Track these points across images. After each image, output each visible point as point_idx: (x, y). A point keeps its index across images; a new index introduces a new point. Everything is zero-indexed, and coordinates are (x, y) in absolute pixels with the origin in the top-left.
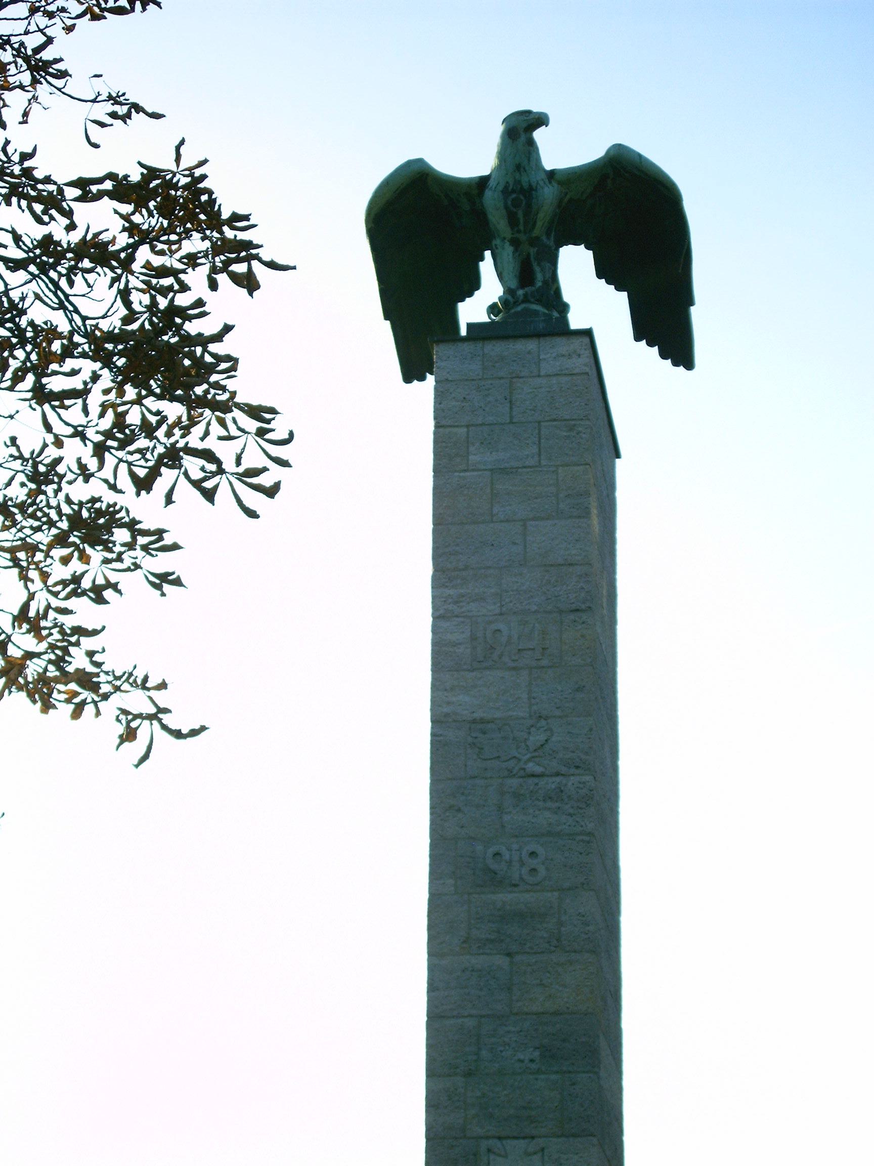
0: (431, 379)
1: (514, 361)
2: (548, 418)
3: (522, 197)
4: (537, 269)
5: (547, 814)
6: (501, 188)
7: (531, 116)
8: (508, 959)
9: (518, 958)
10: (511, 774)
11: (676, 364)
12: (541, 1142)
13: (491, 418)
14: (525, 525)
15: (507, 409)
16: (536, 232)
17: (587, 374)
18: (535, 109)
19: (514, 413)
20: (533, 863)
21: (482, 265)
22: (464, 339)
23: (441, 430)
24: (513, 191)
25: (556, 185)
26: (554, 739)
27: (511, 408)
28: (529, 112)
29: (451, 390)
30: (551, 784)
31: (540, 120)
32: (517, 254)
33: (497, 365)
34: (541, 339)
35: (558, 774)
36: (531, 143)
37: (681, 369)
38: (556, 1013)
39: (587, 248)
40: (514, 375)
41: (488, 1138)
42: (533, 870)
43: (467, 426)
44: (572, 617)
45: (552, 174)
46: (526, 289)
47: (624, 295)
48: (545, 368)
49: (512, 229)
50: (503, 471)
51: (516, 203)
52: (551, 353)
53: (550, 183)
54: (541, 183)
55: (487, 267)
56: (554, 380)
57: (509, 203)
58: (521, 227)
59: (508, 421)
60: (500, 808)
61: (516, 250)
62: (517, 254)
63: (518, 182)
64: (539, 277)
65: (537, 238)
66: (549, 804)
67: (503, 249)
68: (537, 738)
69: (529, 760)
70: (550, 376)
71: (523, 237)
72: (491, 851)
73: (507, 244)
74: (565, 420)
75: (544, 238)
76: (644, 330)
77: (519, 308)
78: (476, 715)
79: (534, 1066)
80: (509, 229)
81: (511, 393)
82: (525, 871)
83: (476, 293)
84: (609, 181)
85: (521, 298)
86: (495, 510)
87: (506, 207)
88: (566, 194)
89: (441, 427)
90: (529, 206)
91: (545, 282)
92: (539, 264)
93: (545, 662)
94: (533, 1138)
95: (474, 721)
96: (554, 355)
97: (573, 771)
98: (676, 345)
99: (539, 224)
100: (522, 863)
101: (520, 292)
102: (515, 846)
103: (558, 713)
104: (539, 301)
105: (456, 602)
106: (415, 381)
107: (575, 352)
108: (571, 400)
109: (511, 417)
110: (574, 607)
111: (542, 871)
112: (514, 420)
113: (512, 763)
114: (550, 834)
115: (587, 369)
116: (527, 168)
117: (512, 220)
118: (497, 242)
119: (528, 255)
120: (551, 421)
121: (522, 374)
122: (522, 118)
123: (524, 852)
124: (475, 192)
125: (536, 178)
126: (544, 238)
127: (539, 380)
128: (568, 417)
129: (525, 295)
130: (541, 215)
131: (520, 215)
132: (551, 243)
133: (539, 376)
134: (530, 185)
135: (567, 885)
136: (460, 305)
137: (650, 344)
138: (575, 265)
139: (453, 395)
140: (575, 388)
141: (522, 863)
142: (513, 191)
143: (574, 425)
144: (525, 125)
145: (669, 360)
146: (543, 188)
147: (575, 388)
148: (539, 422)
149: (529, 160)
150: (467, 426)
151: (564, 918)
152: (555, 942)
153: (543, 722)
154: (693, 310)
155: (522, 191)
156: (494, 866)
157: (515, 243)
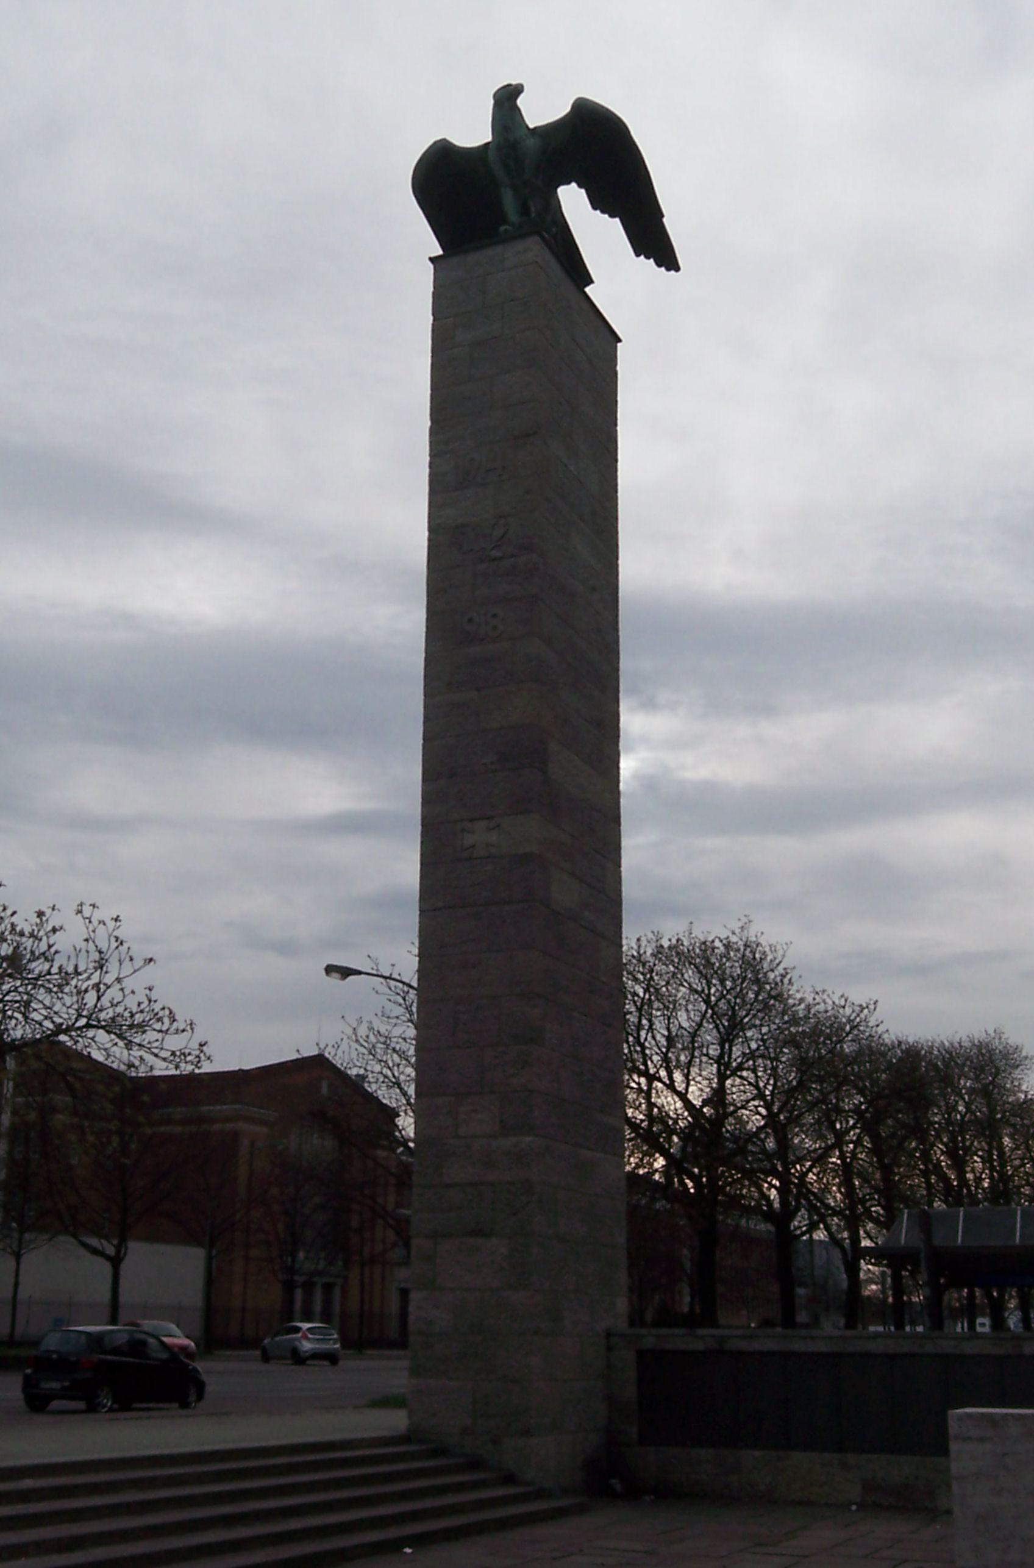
11: (668, 269)
18: (514, 83)
31: (518, 90)
35: (512, 556)
37: (673, 272)
42: (495, 628)
47: (617, 220)
137: (647, 257)
154: (664, 220)
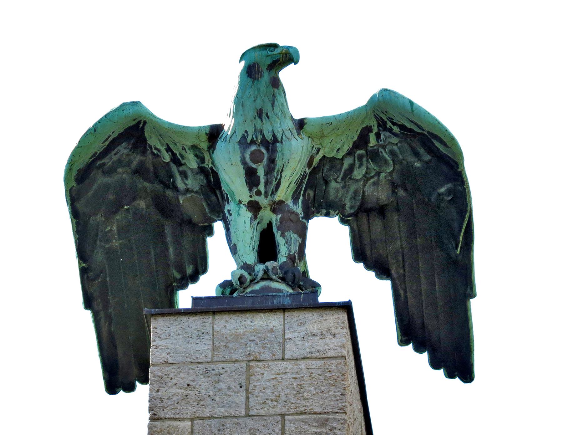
0: (142, 391)
1: (253, 341)
2: (294, 411)
3: (264, 150)
6: (238, 137)
7: (277, 51)
11: (450, 375)
13: (222, 410)
15: (244, 399)
16: (280, 195)
17: (344, 357)
18: (282, 43)
19: (251, 404)
21: (210, 241)
22: (186, 313)
23: (158, 423)
24: (253, 142)
25: (306, 138)
27: (247, 398)
28: (275, 46)
29: (171, 375)
31: (288, 57)
32: (256, 222)
33: (230, 345)
34: (287, 314)
36: (276, 83)
40: (252, 358)
43: (192, 420)
45: (301, 124)
46: (268, 264)
47: (387, 285)
48: (291, 350)
49: (250, 190)
52: (301, 331)
53: (299, 134)
54: (288, 134)
55: (216, 244)
56: (302, 364)
57: (247, 157)
58: (262, 188)
59: (243, 413)
62: (256, 222)
65: (281, 202)
67: (239, 214)
70: (297, 359)
71: (263, 201)
74: (315, 413)
75: (290, 202)
76: (411, 332)
77: (257, 287)
80: (246, 189)
81: (248, 379)
85: (261, 274)
87: (244, 162)
88: (318, 151)
89: (159, 419)
90: (272, 161)
91: (291, 258)
92: (283, 235)
96: (302, 334)
98: (450, 350)
99: (284, 185)
101: (260, 268)
104: (283, 279)
106: (122, 392)
107: (329, 330)
108: (323, 388)
109: (248, 409)
112: (251, 413)
115: (345, 352)
116: (270, 115)
117: (251, 178)
118: (230, 207)
119: (270, 224)
120: (297, 414)
121: (263, 357)
122: (264, 53)
125: (283, 127)
126: (290, 202)
127: (284, 364)
128: (319, 410)
129: (266, 272)
130: (287, 173)
131: (261, 172)
132: (299, 209)
133: (283, 359)
134: (274, 136)
137: (419, 349)
138: (328, 249)
139: (174, 381)
140: (328, 375)
142: (253, 142)
143: (327, 420)
144: (269, 61)
145: (442, 371)
146: (289, 140)
147: (328, 375)
148: (283, 416)
149: (273, 104)
150: (192, 420)
154: (473, 302)
155: (264, 143)
157: (254, 207)
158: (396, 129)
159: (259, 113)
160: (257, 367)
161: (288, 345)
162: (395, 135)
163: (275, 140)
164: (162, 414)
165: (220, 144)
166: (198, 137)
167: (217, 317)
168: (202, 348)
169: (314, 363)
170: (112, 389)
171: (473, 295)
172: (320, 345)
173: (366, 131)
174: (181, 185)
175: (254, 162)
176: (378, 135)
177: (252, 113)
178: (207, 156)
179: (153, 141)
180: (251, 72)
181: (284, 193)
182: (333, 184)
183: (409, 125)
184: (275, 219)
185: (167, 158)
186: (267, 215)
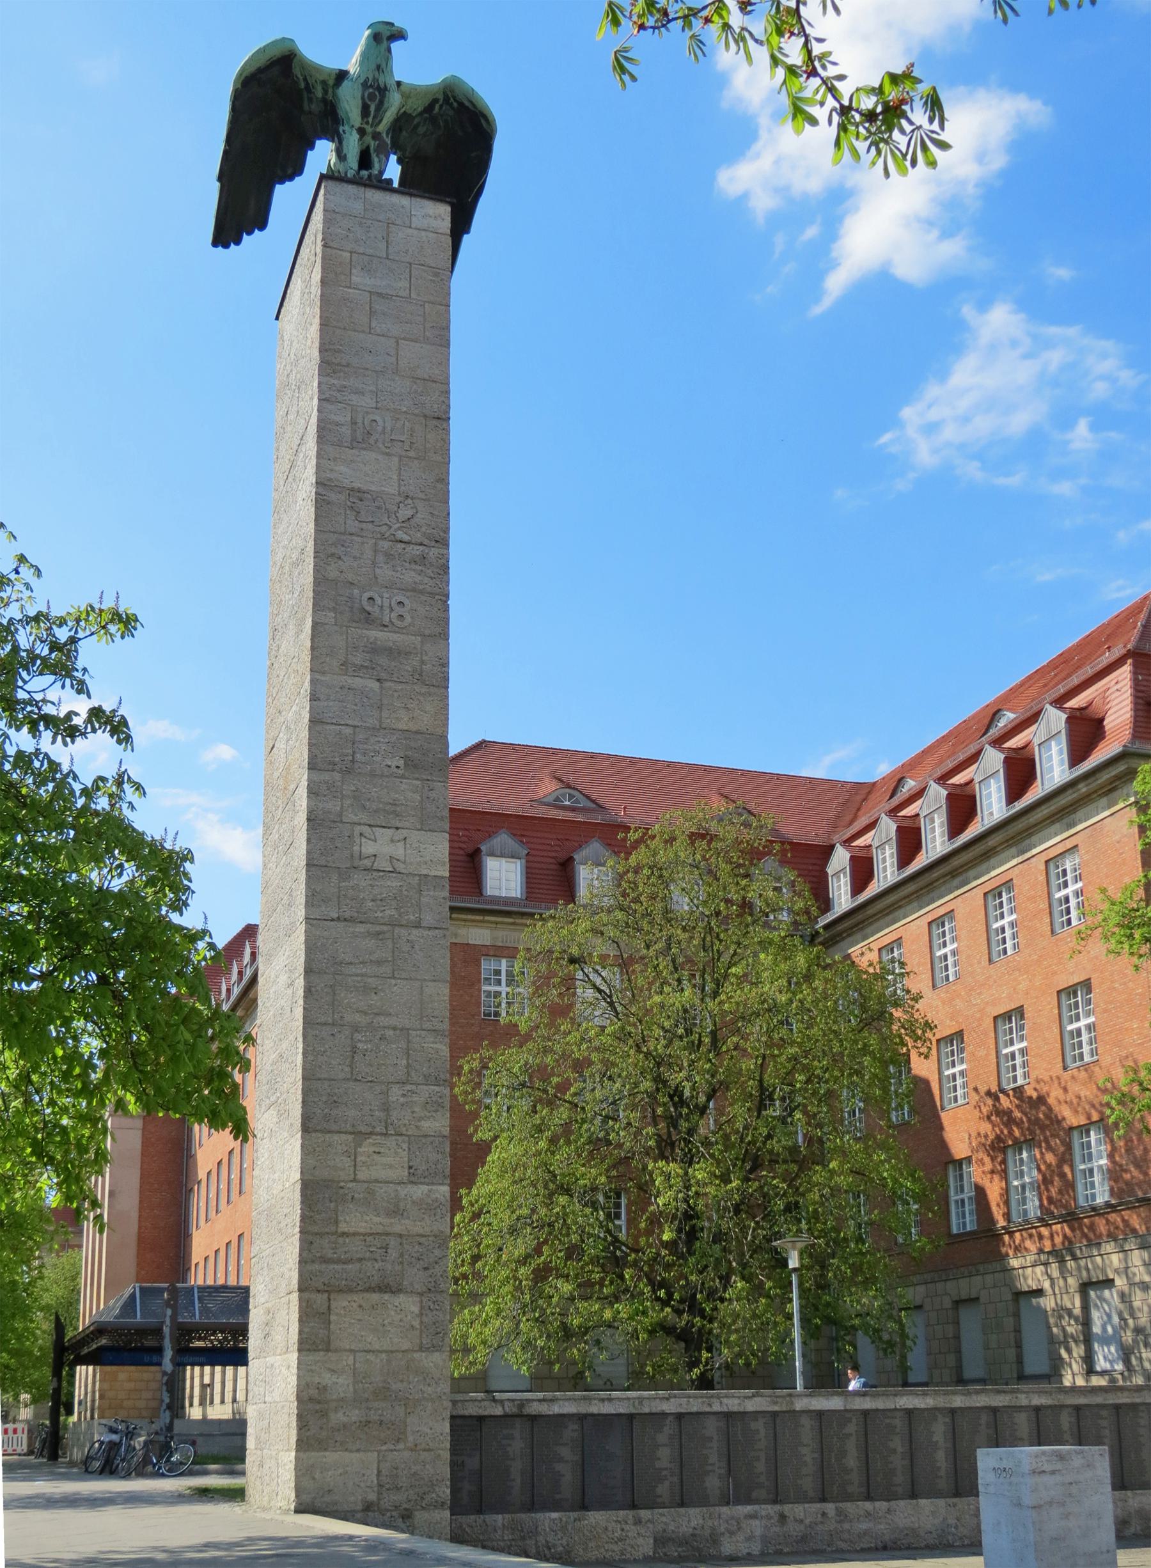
4: (376, 160)
5: (413, 574)
8: (378, 684)
9: (387, 684)
10: (383, 537)
12: (403, 833)
14: (397, 342)
20: (399, 610)
24: (371, 86)
26: (419, 515)
30: (417, 550)
35: (421, 544)
36: (389, 50)
38: (417, 732)
39: (250, 233)
41: (360, 824)
44: (435, 422)
45: (399, 84)
50: (380, 295)
51: (372, 97)
56: (423, 233)
58: (370, 120)
60: (374, 563)
61: (361, 139)
63: (376, 80)
64: (377, 166)
65: (379, 133)
66: (414, 566)
68: (405, 513)
69: (399, 529)
71: (369, 129)
72: (367, 595)
73: (355, 132)
75: (384, 135)
78: (354, 485)
79: (400, 772)
82: (394, 615)
83: (287, 183)
84: (437, 107)
86: (373, 325)
87: (363, 98)
90: (381, 103)
93: (412, 454)
94: (397, 828)
95: (352, 490)
97: (433, 544)
99: (385, 121)
100: (392, 610)
102: (386, 595)
103: (422, 496)
105: (339, 391)
110: (436, 415)
111: (408, 620)
113: (384, 528)
114: (414, 590)
119: (368, 148)
123: (393, 603)
124: (331, 82)
126: (384, 135)
127: (410, 231)
131: (372, 109)
135: (427, 632)
136: (278, 187)
141: (392, 610)
142: (371, 86)
144: (388, 34)
151: (425, 658)
152: (417, 677)
153: (410, 501)
155: (379, 88)
156: (368, 608)
157: (361, 132)
158: (455, 105)
159: (378, 67)
160: (393, 228)
161: (414, 219)
162: (453, 108)
163: (386, 88)
164: (331, 244)
165: (345, 83)
166: (330, 75)
167: (368, 190)
168: (358, 207)
169: (431, 235)
170: (215, 243)
171: (468, 232)
172: (435, 224)
173: (435, 101)
174: (306, 107)
175: (370, 100)
176: (441, 106)
177: (374, 66)
178: (330, 91)
179: (296, 71)
180: (376, 37)
181: (382, 128)
182: (404, 133)
183: (467, 104)
184: (373, 144)
185: (302, 85)
186: (368, 139)
